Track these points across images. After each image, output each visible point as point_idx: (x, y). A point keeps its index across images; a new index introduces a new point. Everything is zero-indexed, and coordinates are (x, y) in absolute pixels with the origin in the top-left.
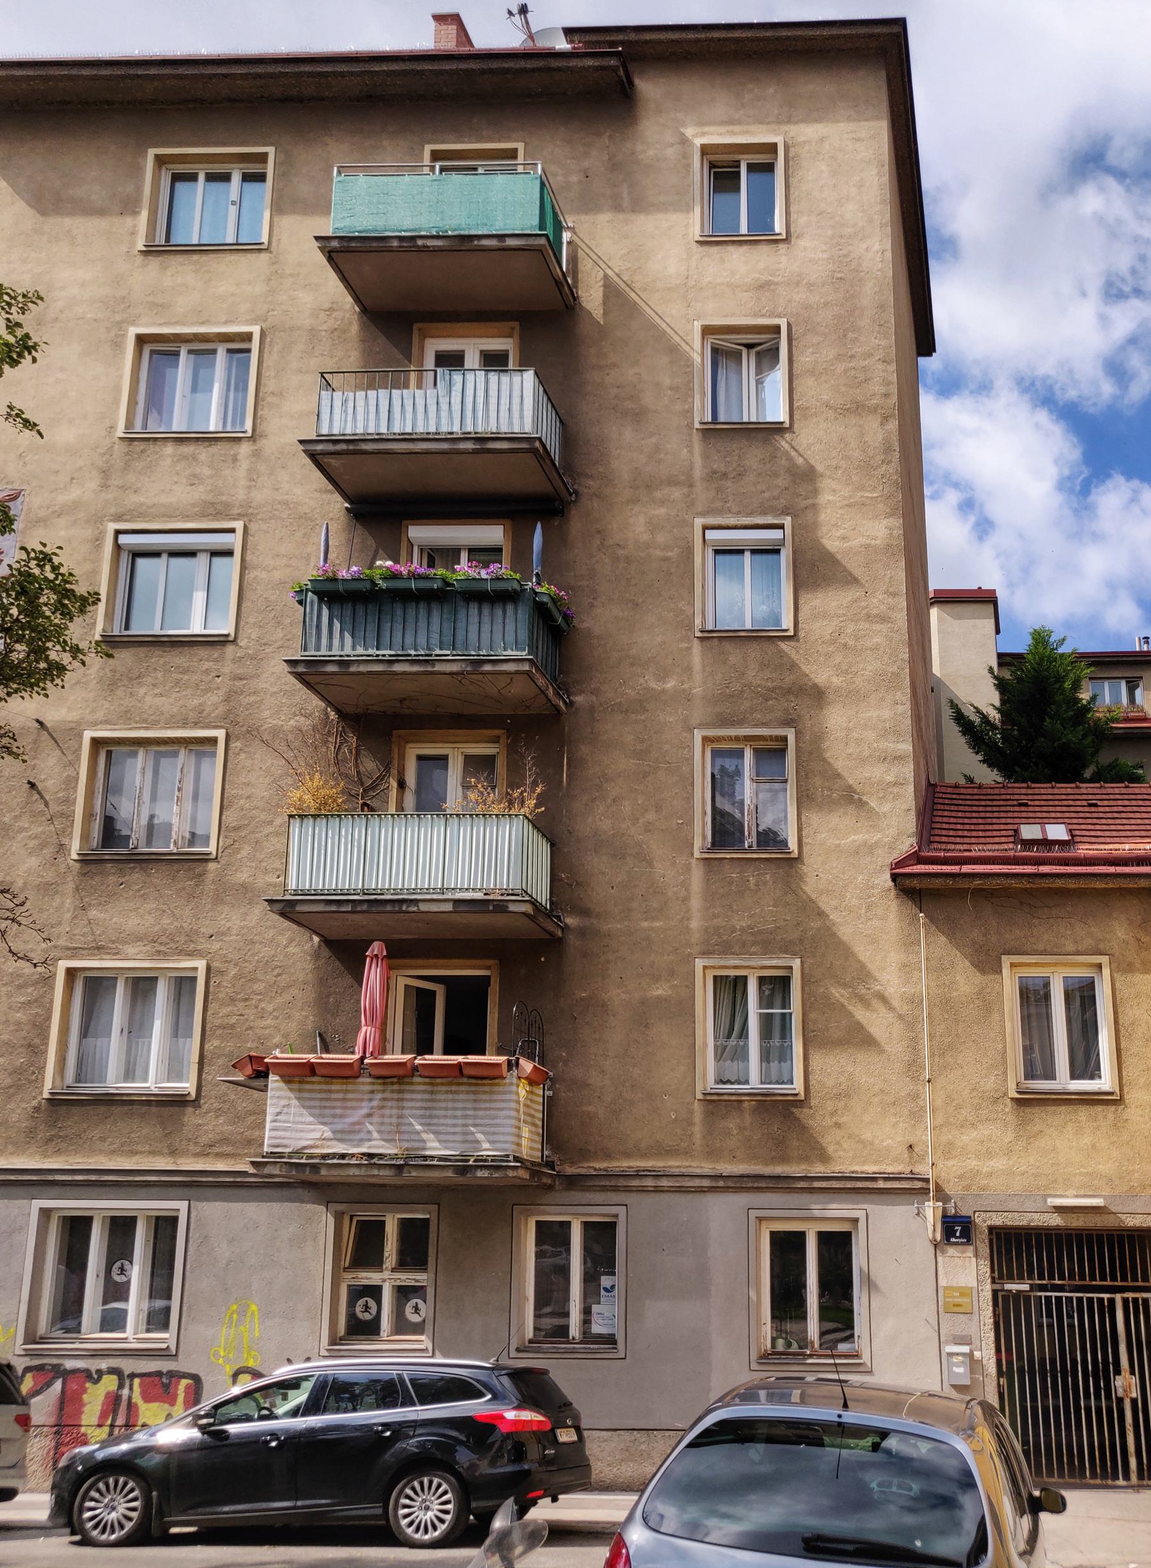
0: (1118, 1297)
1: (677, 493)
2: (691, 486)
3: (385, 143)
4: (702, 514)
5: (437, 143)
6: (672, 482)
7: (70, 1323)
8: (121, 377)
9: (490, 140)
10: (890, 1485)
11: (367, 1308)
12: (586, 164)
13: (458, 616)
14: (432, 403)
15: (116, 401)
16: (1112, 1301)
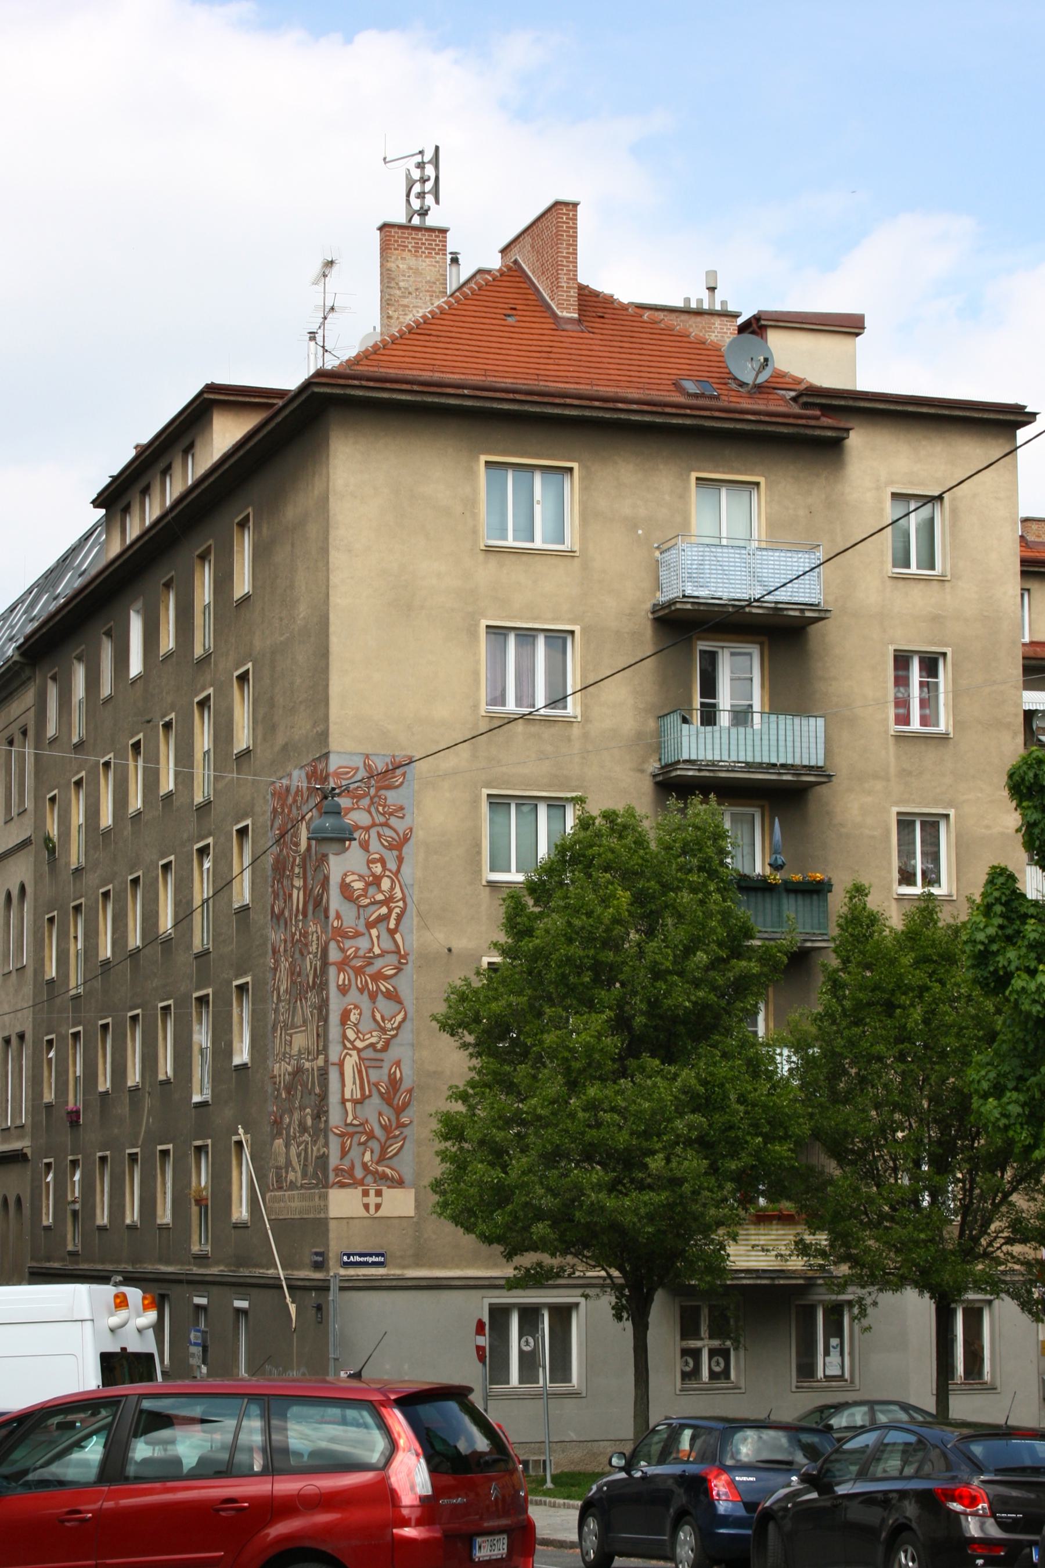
1: (879, 785)
2: (888, 780)
3: (661, 467)
4: (896, 803)
5: (704, 471)
6: (876, 776)
7: (1016, 778)
10: (526, 1135)
11: (718, 1364)
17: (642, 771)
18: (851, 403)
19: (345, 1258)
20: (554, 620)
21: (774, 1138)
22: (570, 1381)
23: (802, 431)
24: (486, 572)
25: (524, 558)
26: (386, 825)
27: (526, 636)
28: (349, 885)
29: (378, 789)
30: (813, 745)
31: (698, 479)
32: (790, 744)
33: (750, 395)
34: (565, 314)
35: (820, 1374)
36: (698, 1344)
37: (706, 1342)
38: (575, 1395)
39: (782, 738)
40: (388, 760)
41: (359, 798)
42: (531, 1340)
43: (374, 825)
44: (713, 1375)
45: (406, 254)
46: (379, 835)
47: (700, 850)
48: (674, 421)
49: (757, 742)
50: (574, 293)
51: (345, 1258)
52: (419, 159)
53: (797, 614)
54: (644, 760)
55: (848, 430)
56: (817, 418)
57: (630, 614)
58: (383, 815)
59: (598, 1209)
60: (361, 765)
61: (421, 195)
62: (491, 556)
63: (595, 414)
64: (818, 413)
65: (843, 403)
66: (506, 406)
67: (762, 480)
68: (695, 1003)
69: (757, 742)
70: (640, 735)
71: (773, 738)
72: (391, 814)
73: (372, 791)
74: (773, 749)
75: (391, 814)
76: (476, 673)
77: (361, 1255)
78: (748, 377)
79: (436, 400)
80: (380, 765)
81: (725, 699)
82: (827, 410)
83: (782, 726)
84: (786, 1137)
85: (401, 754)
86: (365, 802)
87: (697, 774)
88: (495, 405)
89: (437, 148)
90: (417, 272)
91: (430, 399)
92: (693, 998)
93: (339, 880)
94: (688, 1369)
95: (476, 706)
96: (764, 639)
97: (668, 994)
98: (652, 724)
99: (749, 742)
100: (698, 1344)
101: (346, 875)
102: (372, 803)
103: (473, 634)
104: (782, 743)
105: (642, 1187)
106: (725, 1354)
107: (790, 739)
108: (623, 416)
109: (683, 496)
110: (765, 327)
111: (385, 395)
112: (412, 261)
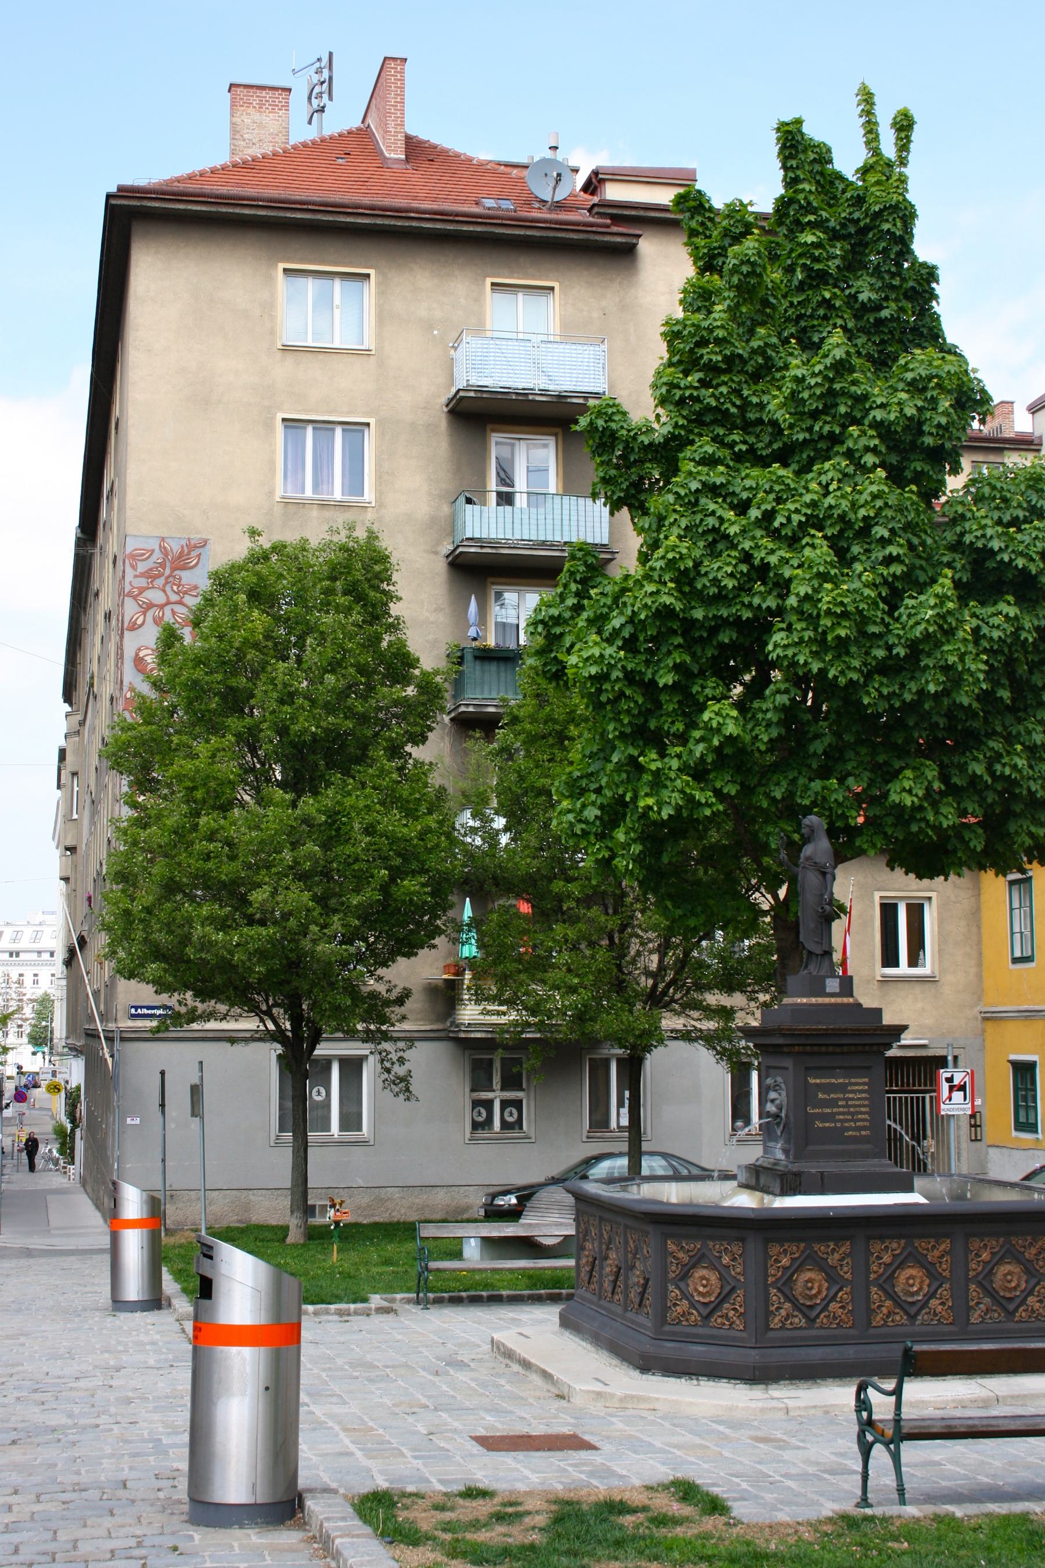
0: (927, 1096)
3: (457, 273)
8: (274, 452)
9: (534, 278)
11: (511, 1114)
12: (604, 303)
13: (984, 898)
14: (541, 517)
15: (273, 470)
16: (924, 1098)
17: (436, 553)
18: (642, 213)
19: (133, 1011)
20: (350, 413)
21: (407, 874)
22: (360, 1129)
23: (592, 237)
24: (283, 370)
25: (321, 356)
26: (180, 602)
27: (324, 426)
28: (142, 659)
29: (173, 569)
30: (597, 525)
31: (493, 284)
32: (574, 523)
33: (550, 210)
34: (392, 156)
35: (613, 1124)
36: (489, 1095)
37: (498, 1093)
38: (364, 1143)
39: (566, 517)
40: (184, 542)
41: (155, 577)
42: (323, 1091)
43: (168, 603)
44: (505, 1125)
45: (250, 110)
46: (174, 613)
47: (349, 573)
48: (465, 228)
49: (541, 522)
50: (401, 137)
51: (133, 1011)
52: (317, 65)
53: (581, 401)
54: (439, 543)
55: (639, 236)
56: (608, 227)
57: (424, 408)
58: (177, 593)
59: (206, 945)
60: (157, 548)
61: (320, 95)
62: (288, 354)
63: (387, 222)
64: (608, 221)
65: (633, 213)
66: (299, 215)
67: (556, 285)
68: (326, 730)
69: (541, 522)
70: (433, 520)
71: (558, 517)
72: (185, 593)
73: (168, 572)
74: (558, 527)
75: (185, 593)
76: (272, 463)
77: (148, 1008)
78: (547, 196)
79: (231, 210)
80: (175, 547)
81: (521, 483)
82: (616, 219)
83: (566, 506)
84: (423, 871)
85: (195, 537)
86: (160, 582)
87: (479, 550)
88: (289, 215)
89: (331, 54)
90: (261, 125)
91: (224, 209)
92: (324, 724)
93: (133, 654)
94: (480, 1119)
95: (271, 493)
96: (559, 430)
97: (294, 719)
98: (446, 509)
99: (533, 522)
100: (489, 1095)
101: (139, 649)
102: (167, 583)
103: (269, 426)
104: (566, 522)
105: (251, 921)
106: (518, 1104)
107: (574, 518)
108: (414, 224)
109: (479, 300)
110: (603, 181)
111: (181, 206)
112: (257, 117)
